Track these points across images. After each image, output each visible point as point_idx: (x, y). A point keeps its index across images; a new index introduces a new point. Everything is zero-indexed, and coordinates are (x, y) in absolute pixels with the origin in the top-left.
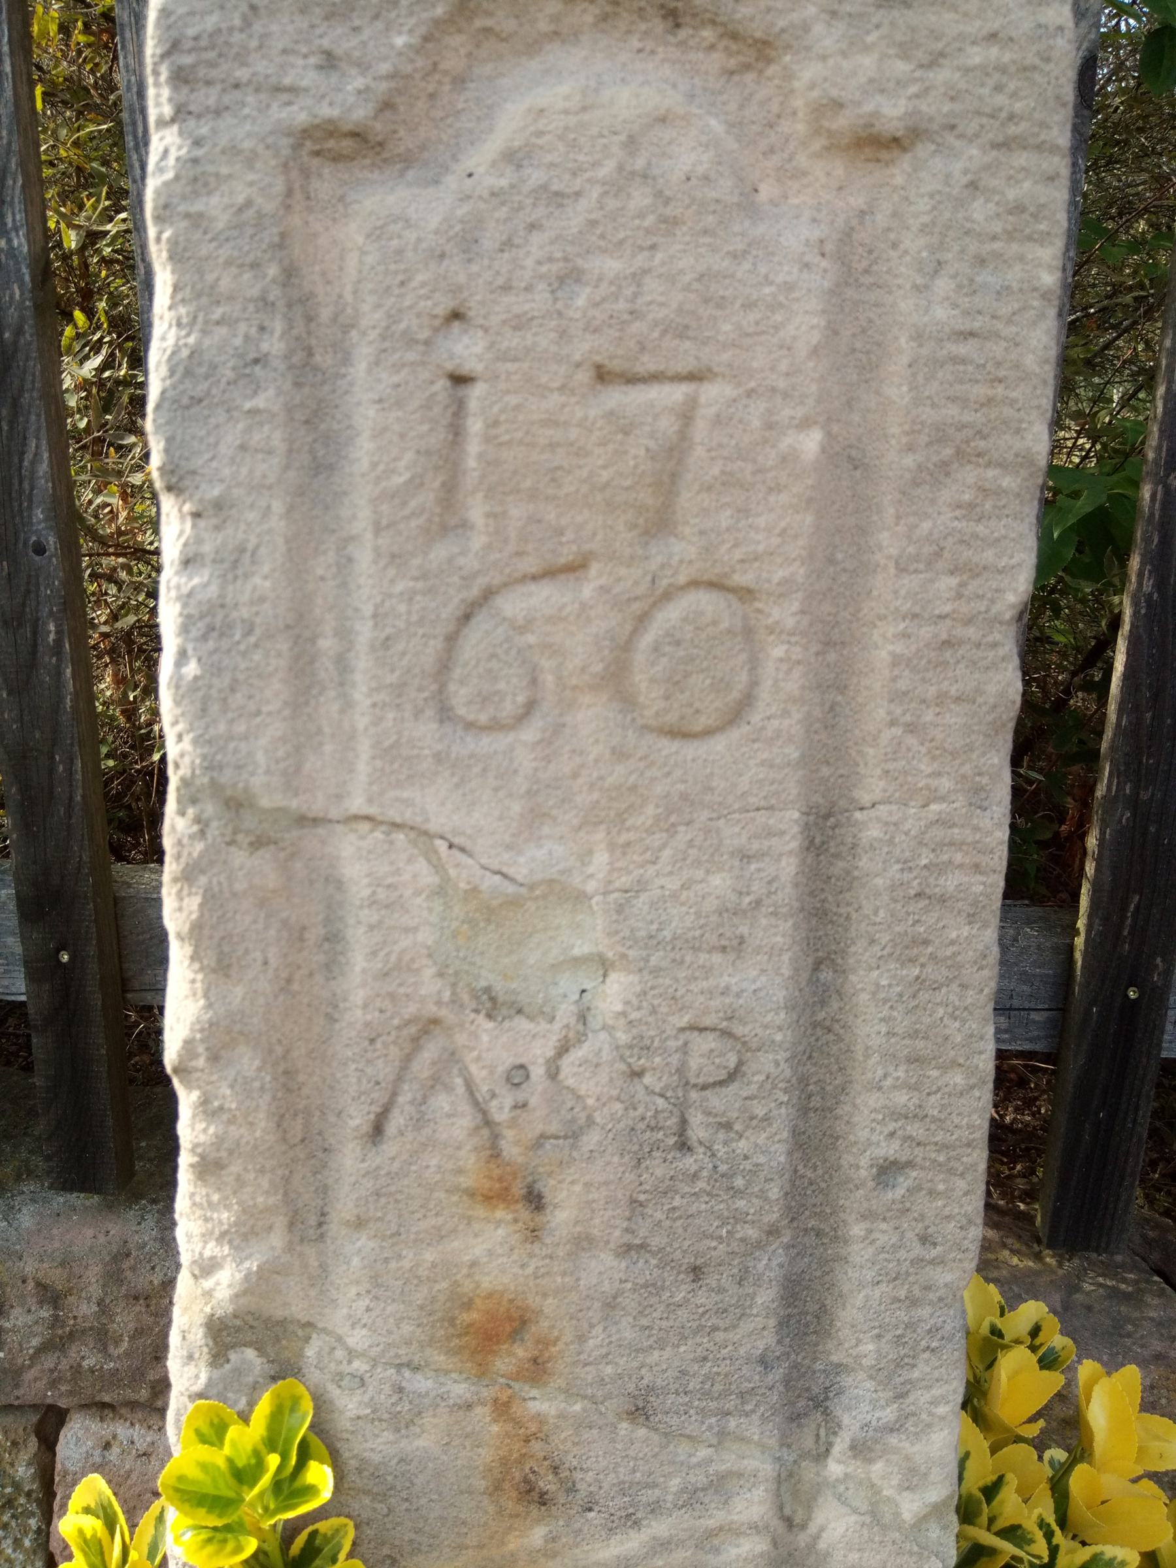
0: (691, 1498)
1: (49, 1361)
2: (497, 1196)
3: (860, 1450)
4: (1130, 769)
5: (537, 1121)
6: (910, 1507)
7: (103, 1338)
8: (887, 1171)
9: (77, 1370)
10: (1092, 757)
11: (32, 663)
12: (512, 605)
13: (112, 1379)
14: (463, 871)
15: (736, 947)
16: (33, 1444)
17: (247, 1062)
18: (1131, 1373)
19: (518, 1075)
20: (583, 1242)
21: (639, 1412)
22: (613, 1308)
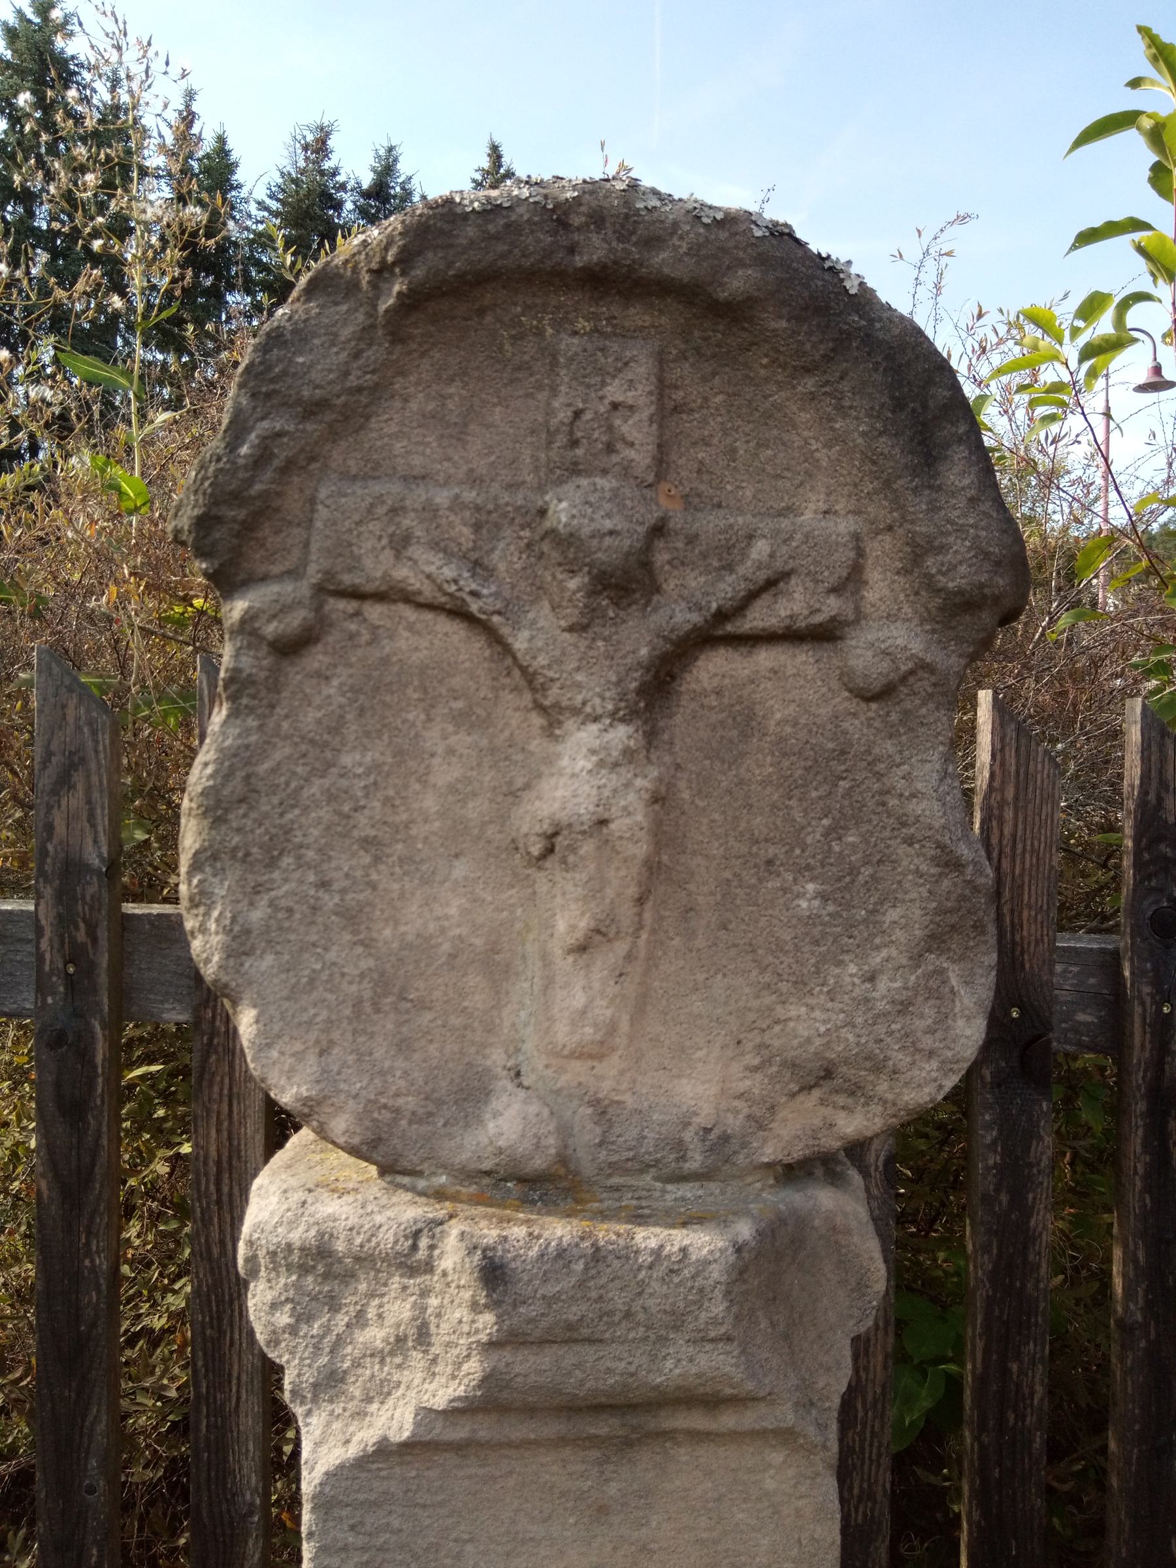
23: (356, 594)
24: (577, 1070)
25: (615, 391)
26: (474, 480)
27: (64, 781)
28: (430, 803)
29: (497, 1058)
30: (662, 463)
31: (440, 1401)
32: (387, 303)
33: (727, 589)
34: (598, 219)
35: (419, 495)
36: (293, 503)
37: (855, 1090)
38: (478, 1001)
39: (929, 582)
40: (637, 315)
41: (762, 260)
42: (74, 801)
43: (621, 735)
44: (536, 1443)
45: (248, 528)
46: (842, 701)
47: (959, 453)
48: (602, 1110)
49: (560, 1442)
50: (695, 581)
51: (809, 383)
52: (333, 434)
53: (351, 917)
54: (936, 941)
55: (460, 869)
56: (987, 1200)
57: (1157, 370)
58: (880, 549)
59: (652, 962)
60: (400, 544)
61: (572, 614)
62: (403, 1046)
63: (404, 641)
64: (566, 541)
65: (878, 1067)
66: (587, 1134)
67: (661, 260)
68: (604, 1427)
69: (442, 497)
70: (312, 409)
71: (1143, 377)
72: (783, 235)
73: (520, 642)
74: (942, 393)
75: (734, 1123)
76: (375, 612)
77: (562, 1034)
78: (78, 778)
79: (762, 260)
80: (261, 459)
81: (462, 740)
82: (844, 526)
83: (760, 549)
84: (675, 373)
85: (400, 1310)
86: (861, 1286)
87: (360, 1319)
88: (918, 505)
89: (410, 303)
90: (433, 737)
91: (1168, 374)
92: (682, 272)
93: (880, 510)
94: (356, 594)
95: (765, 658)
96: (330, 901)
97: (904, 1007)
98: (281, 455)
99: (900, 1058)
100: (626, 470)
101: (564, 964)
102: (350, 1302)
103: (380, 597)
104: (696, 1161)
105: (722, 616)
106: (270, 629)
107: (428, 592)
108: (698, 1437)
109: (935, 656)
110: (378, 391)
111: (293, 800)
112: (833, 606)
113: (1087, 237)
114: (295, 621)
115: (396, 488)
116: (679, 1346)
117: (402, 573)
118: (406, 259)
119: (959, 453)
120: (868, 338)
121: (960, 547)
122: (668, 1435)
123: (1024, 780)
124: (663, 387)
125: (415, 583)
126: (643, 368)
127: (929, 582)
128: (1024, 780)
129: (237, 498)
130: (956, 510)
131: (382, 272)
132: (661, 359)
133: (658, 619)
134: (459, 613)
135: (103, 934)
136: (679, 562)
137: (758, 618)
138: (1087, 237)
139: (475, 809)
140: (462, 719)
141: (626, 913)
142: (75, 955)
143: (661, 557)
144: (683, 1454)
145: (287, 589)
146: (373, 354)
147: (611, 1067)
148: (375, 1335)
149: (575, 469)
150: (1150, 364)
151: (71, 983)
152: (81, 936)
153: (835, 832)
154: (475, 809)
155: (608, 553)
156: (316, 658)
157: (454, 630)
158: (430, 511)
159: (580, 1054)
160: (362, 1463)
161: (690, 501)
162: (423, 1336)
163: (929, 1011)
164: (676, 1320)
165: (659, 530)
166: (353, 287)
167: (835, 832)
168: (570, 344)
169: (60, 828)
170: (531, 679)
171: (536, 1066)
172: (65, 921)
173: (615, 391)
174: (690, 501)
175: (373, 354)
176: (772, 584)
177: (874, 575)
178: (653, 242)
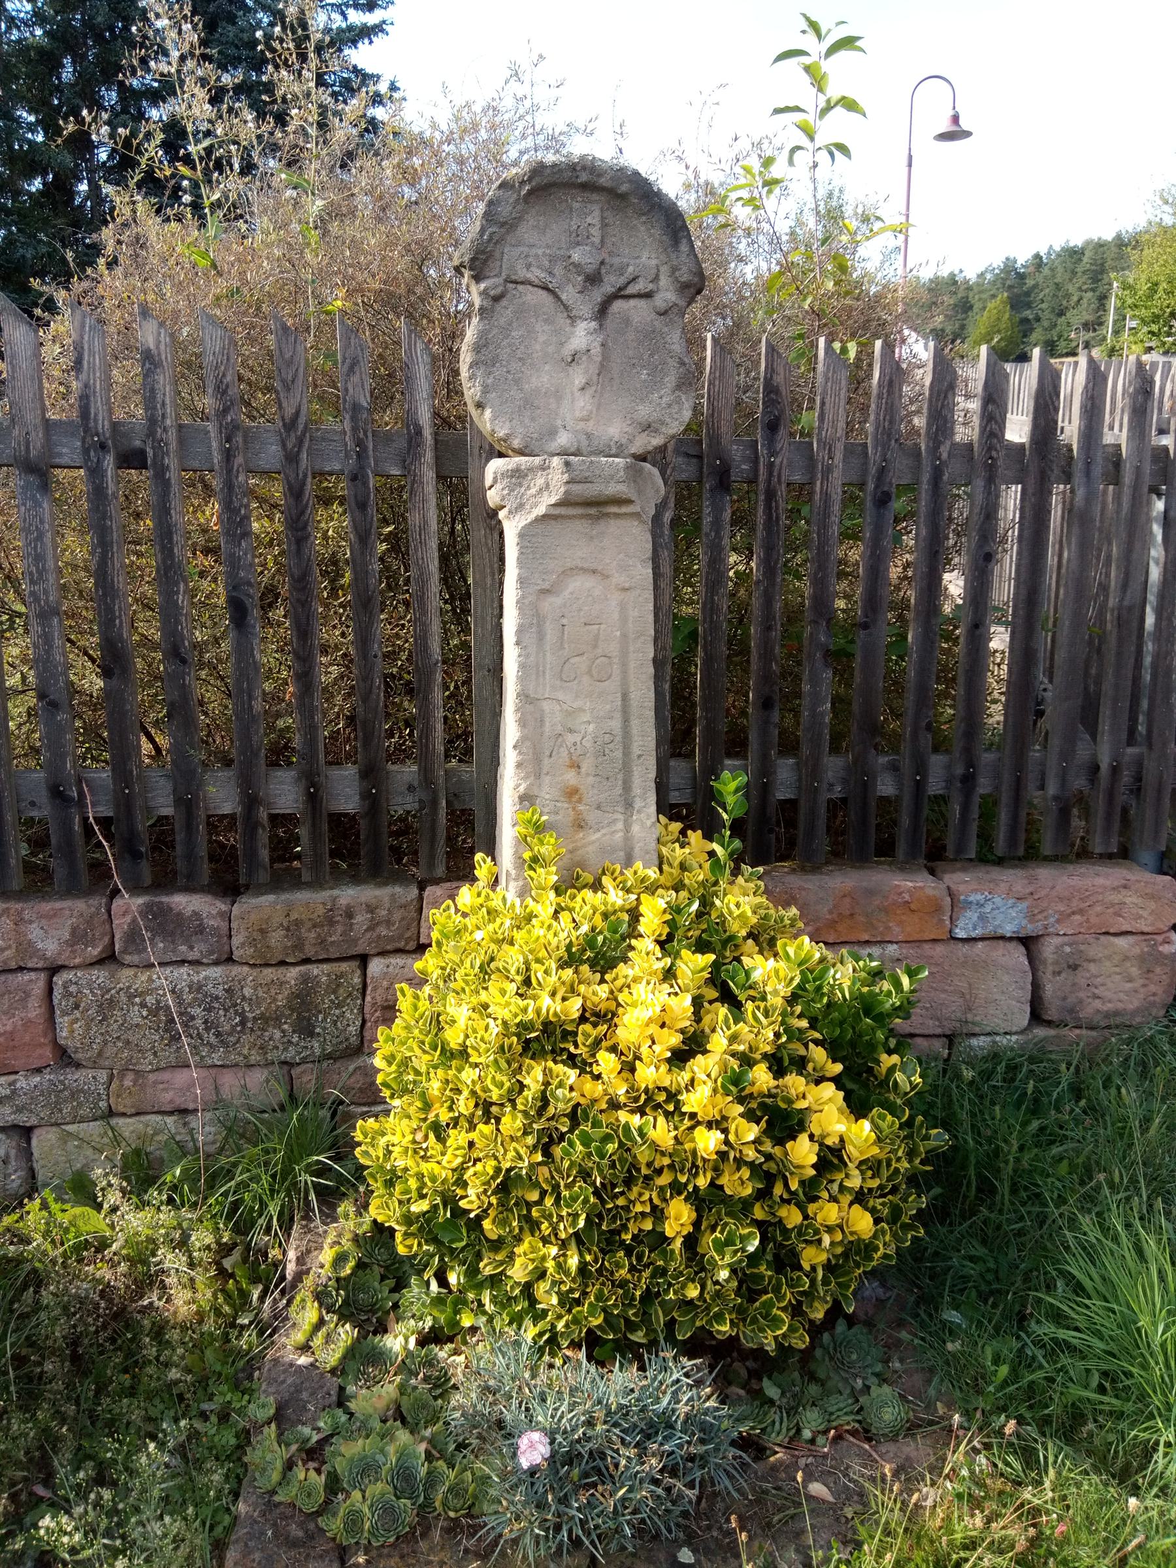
0: (609, 824)
1: (368, 935)
2: (572, 766)
3: (639, 812)
4: (705, 709)
5: (579, 752)
6: (649, 823)
7: (388, 923)
8: (640, 756)
9: (379, 937)
10: (694, 705)
11: (370, 691)
12: (572, 661)
13: (391, 939)
14: (565, 707)
15: (611, 718)
16: (359, 972)
17: (528, 744)
18: (699, 832)
19: (575, 744)
20: (588, 775)
21: (598, 808)
22: (487, 1117)
23: (516, 282)
24: (582, 425)
25: (589, 220)
26: (548, 247)
27: (351, 369)
28: (538, 347)
29: (559, 422)
30: (602, 241)
31: (553, 501)
32: (523, 192)
33: (622, 281)
34: (584, 168)
35: (534, 251)
36: (497, 254)
37: (656, 431)
38: (553, 406)
39: (676, 279)
40: (595, 197)
41: (630, 181)
42: (355, 379)
43: (594, 324)
44: (574, 516)
45: (486, 261)
46: (653, 316)
47: (684, 241)
48: (589, 436)
49: (582, 517)
50: (613, 278)
51: (644, 218)
52: (508, 232)
53: (517, 382)
54: (679, 387)
55: (547, 367)
56: (707, 535)
57: (955, 119)
58: (664, 269)
59: (602, 395)
60: (528, 266)
61: (579, 288)
62: (533, 419)
63: (529, 297)
64: (577, 266)
65: (663, 423)
66: (585, 443)
67: (602, 181)
68: (593, 511)
69: (540, 252)
70: (503, 225)
71: (945, 126)
72: (636, 173)
73: (564, 297)
74: (680, 223)
75: (624, 441)
76: (520, 287)
77: (578, 414)
78: (356, 369)
79: (630, 181)
80: (490, 240)
81: (546, 328)
82: (654, 262)
83: (631, 269)
84: (610, 220)
85: (540, 481)
86: (657, 491)
87: (529, 488)
88: (674, 256)
89: (530, 192)
90: (538, 328)
91: (965, 124)
92: (608, 184)
93: (663, 257)
94: (516, 282)
95: (632, 302)
96: (510, 377)
97: (669, 406)
98: (495, 239)
99: (668, 420)
100: (593, 243)
101: (577, 394)
102: (525, 483)
103: (522, 283)
104: (613, 451)
105: (620, 289)
106: (492, 293)
107: (537, 282)
108: (617, 515)
109: (679, 302)
110: (520, 219)
111: (498, 346)
112: (651, 286)
113: (777, 111)
114: (499, 290)
115: (526, 249)
116: (612, 484)
117: (529, 275)
118: (530, 179)
119: (684, 241)
120: (660, 206)
121: (684, 269)
122: (608, 515)
123: (723, 369)
124: (603, 218)
125: (533, 279)
126: (597, 213)
127: (676, 279)
128: (723, 369)
129: (483, 252)
130: (683, 257)
131: (522, 183)
132: (602, 210)
133: (603, 290)
134: (545, 288)
135: (370, 434)
136: (608, 273)
137: (631, 290)
138: (777, 111)
139: (551, 349)
140: (545, 321)
141: (595, 378)
142: (359, 443)
143: (603, 271)
144: (612, 522)
145: (496, 280)
146: (519, 207)
147: (591, 423)
148: (533, 491)
149: (578, 244)
150: (952, 113)
151: (358, 454)
152: (361, 435)
153: (651, 355)
154: (551, 349)
155: (590, 269)
156: (504, 302)
157: (544, 293)
158: (537, 256)
159: (582, 420)
160: (531, 524)
161: (611, 254)
162: (548, 485)
163: (676, 407)
164: (612, 477)
165: (602, 263)
166: (513, 186)
167: (651, 355)
168: (576, 205)
169: (351, 391)
170: (566, 307)
171: (570, 423)
172: (355, 429)
173: (589, 220)
174: (611, 254)
175: (519, 207)
176: (634, 279)
177: (662, 277)
178: (600, 175)
